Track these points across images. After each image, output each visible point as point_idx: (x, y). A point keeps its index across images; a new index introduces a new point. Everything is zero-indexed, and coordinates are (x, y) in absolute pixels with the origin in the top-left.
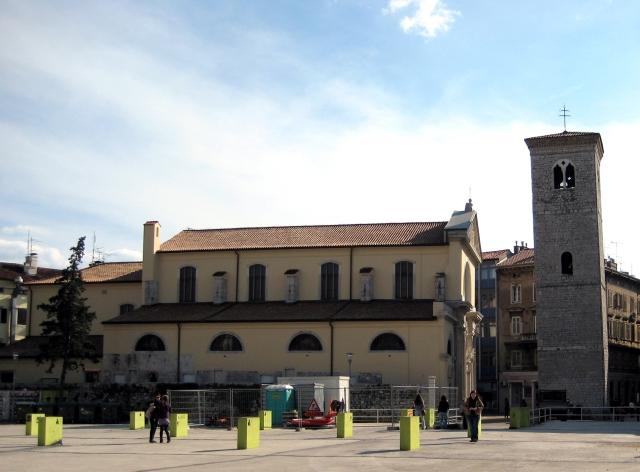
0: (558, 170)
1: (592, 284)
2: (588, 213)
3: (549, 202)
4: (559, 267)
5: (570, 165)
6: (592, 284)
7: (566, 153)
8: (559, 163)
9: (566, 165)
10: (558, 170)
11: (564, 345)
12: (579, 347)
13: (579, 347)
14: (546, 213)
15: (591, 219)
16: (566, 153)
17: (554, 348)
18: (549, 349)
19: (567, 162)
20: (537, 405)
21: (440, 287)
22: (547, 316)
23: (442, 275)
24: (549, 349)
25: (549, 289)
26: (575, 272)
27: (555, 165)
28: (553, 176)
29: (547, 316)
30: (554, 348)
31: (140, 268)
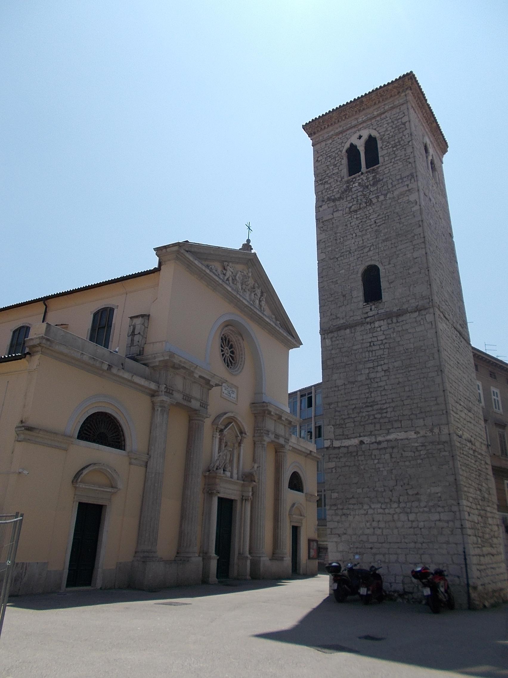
0: (353, 151)
1: (418, 309)
2: (402, 194)
3: (340, 198)
4: (359, 293)
5: (370, 136)
6: (418, 309)
7: (364, 122)
8: (354, 140)
9: (365, 137)
10: (353, 151)
11: (371, 434)
12: (402, 435)
13: (402, 435)
14: (336, 215)
15: (409, 202)
16: (364, 122)
17: (355, 441)
18: (347, 443)
19: (365, 134)
20: (367, 168)
21: (133, 334)
22: (339, 382)
23: (146, 317)
24: (347, 443)
25: (342, 332)
26: (385, 296)
27: (347, 145)
28: (345, 161)
29: (339, 382)
30: (355, 441)
31: (8, 604)
